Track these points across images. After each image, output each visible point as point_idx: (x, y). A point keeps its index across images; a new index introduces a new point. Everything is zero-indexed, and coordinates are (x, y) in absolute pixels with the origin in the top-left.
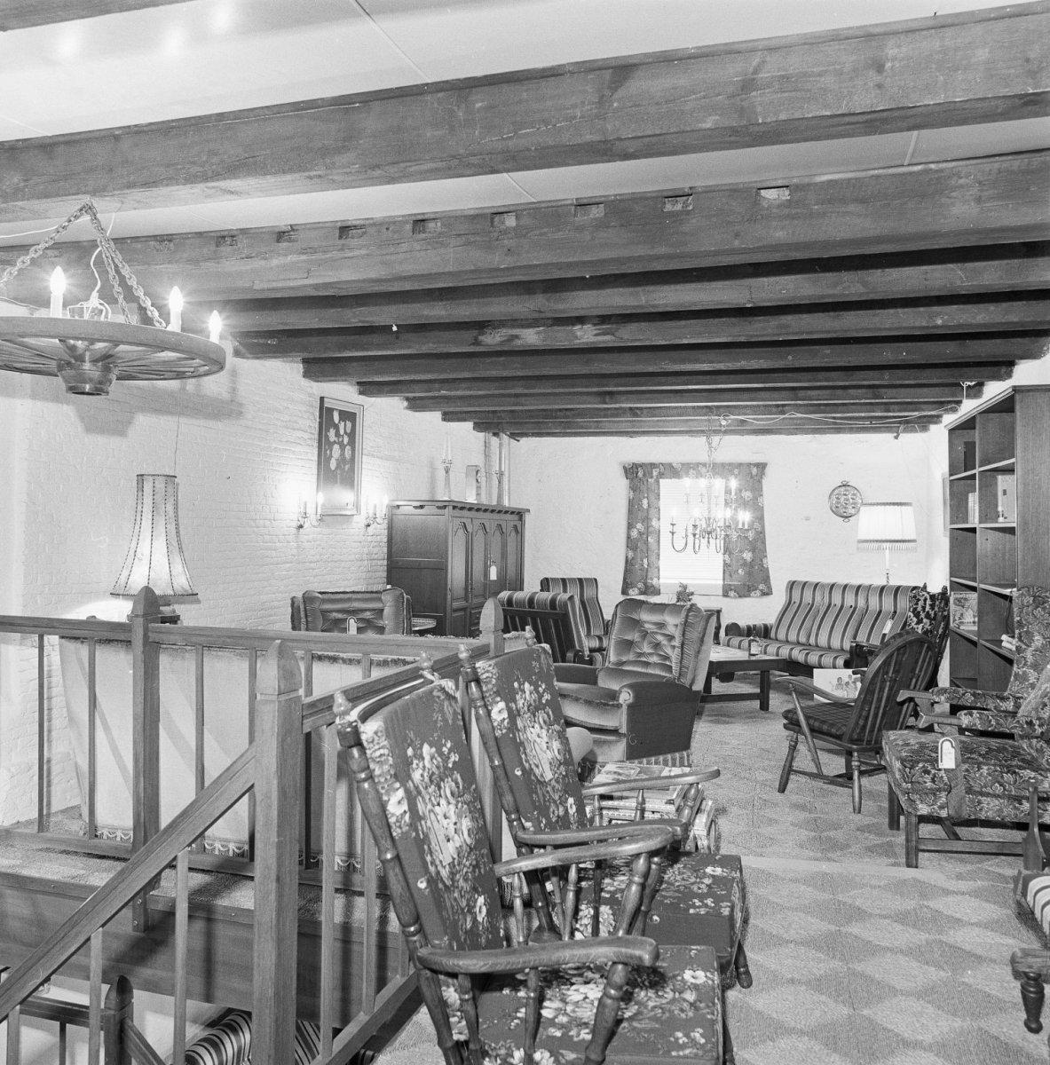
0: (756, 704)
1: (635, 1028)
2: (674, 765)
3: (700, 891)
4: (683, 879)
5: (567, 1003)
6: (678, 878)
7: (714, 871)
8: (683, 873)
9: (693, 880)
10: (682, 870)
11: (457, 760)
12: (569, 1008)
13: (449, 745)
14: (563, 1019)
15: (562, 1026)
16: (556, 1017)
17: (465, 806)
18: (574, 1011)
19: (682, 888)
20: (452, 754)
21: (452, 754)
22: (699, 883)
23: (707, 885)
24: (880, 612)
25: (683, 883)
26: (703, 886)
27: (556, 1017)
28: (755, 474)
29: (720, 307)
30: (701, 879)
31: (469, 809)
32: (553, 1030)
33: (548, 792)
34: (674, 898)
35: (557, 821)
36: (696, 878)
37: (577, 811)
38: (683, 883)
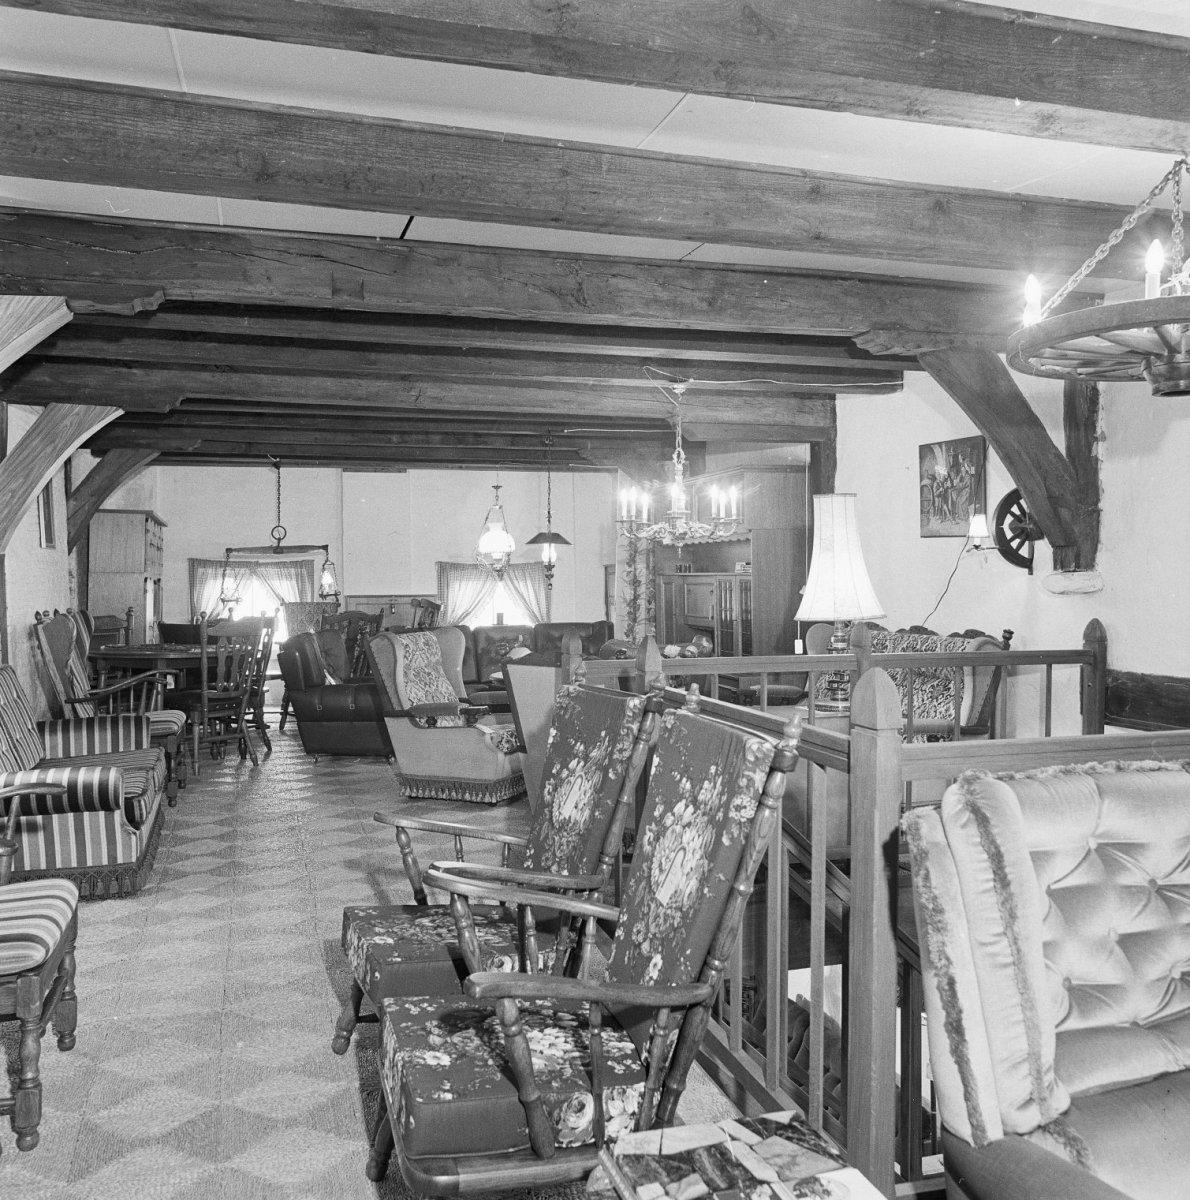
0: (474, 677)
1: (641, 882)
2: (213, 659)
3: (543, 858)
4: (657, 916)
5: (684, 827)
6: (564, 840)
7: (655, 965)
8: (665, 921)
9: (653, 929)
10: (670, 921)
11: (616, 1071)
12: (678, 828)
13: (634, 1066)
14: (669, 820)
15: (662, 816)
16: (673, 815)
17: (558, 1067)
18: (673, 831)
19: (645, 910)
20: (623, 1068)
21: (623, 1068)
22: (646, 934)
23: (640, 944)
24: (876, 730)
25: (557, 845)
26: (640, 938)
27: (673, 815)
28: (195, 564)
29: (849, 1079)
30: (651, 940)
31: (553, 1072)
32: (661, 809)
33: (403, 923)
34: (634, 893)
35: (424, 1029)
36: (654, 935)
37: (376, 944)
38: (557, 845)
